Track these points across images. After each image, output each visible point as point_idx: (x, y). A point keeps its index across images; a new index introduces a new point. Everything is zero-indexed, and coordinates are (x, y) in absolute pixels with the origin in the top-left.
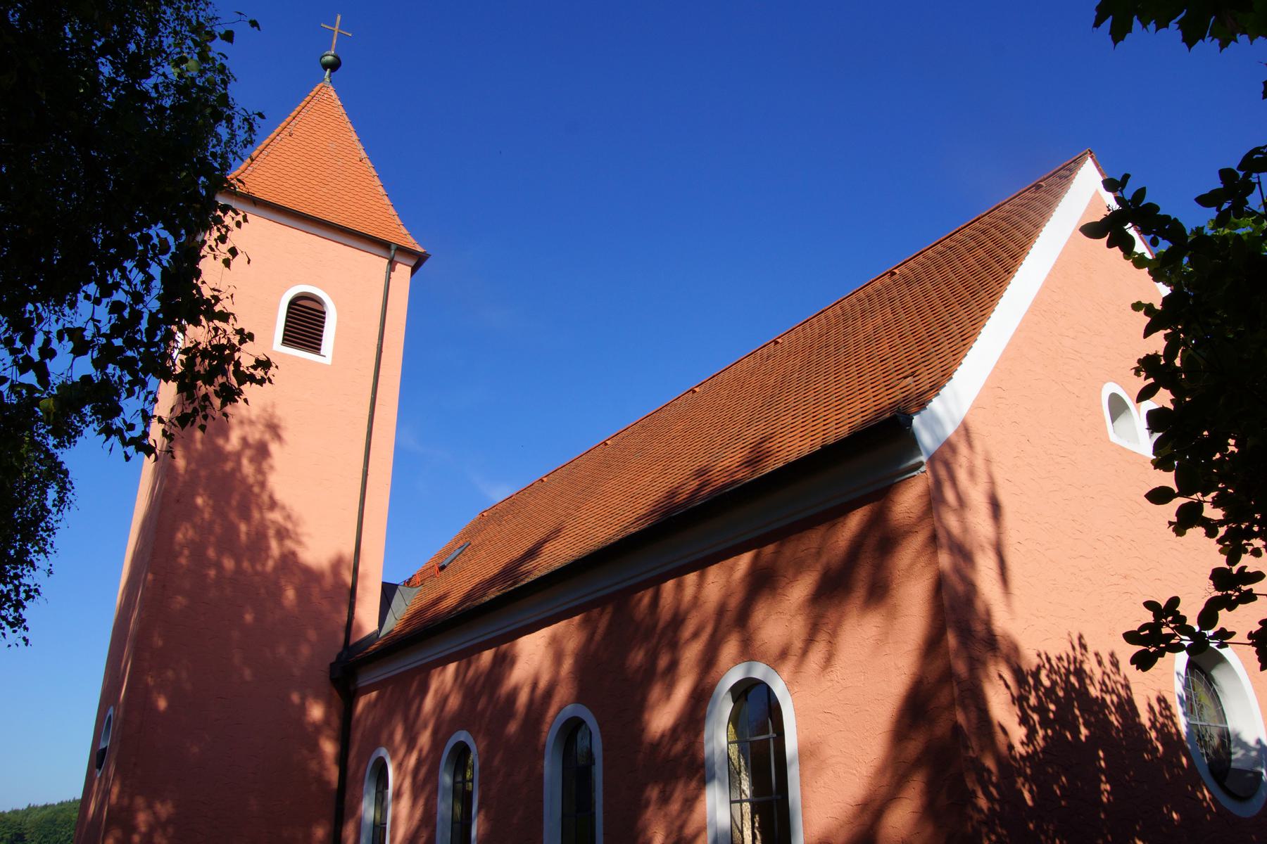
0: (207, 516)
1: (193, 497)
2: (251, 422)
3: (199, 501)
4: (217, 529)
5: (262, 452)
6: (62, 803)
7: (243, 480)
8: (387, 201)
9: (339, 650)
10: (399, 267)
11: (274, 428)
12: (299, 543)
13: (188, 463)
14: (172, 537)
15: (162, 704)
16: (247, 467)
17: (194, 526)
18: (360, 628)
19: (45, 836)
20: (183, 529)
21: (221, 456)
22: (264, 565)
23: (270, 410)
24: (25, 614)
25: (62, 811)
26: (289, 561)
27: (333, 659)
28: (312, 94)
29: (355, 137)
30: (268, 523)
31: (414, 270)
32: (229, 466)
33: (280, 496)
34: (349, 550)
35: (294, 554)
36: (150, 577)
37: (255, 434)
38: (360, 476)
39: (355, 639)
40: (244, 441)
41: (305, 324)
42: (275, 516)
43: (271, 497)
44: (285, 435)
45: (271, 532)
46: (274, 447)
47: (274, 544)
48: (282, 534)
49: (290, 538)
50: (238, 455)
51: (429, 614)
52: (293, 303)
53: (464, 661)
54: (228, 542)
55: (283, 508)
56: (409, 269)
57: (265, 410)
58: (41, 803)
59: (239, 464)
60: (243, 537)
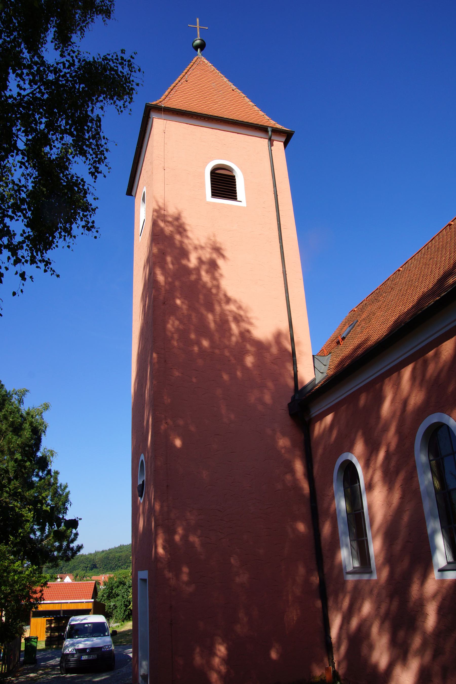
0: (185, 312)
1: (174, 299)
2: (202, 248)
3: (178, 302)
4: (194, 319)
5: (213, 266)
6: (110, 549)
7: (204, 285)
8: (256, 108)
9: (292, 394)
10: (275, 143)
11: (217, 250)
12: (251, 324)
13: (166, 278)
14: (164, 328)
15: (178, 443)
16: (206, 277)
17: (177, 319)
18: (302, 382)
19: (105, 565)
20: (171, 322)
21: (187, 271)
22: (229, 340)
23: (212, 238)
24: (73, 235)
25: (111, 553)
26: (245, 335)
27: (289, 400)
28: (193, 61)
29: (226, 80)
30: (228, 313)
31: (286, 144)
32: (193, 277)
33: (230, 294)
34: (285, 327)
35: (248, 331)
36: (155, 355)
37: (206, 255)
38: (282, 275)
39: (300, 387)
40: (200, 260)
41: (223, 184)
42: (232, 307)
43: (225, 295)
44: (225, 253)
45: (230, 318)
46: (220, 262)
47: (233, 326)
48: (238, 319)
49: (243, 321)
50: (197, 270)
51: (360, 352)
52: (213, 173)
53: (420, 361)
54: (203, 330)
55: (235, 301)
56: (282, 144)
57: (209, 239)
58: (101, 550)
59: (199, 275)
60: (212, 325)
